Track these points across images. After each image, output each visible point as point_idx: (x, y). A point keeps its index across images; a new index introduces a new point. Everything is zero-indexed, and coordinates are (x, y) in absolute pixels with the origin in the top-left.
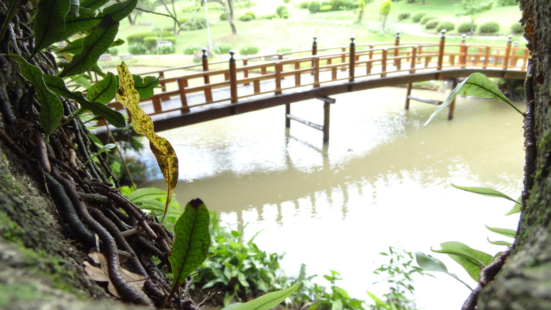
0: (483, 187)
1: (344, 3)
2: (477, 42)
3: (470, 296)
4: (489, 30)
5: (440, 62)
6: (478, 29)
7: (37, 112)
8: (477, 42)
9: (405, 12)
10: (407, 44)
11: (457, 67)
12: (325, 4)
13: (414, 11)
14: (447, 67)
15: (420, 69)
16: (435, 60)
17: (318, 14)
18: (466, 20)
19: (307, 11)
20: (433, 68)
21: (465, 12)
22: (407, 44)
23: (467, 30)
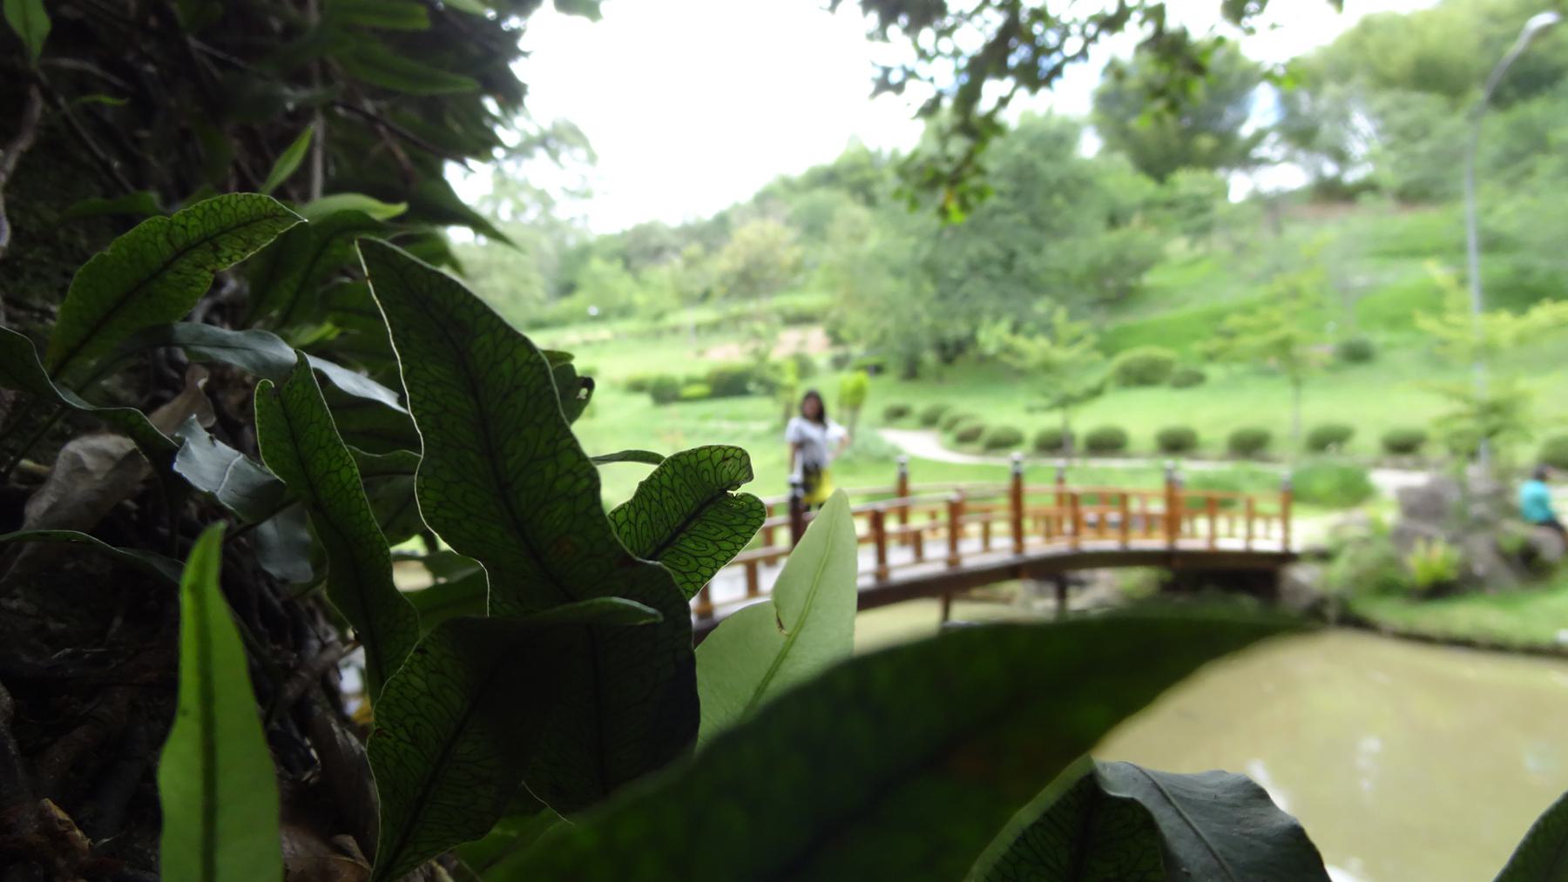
0: (1062, 774)
1: (1257, 66)
2: (1089, 474)
3: (624, 234)
4: (1107, 444)
5: (1018, 533)
6: (1080, 444)
7: (62, 626)
8: (1089, 474)
9: (897, 400)
10: (931, 491)
11: (1061, 546)
12: (691, 381)
13: (920, 401)
14: (1036, 546)
15: (973, 554)
16: (1001, 528)
17: (676, 409)
18: (1051, 421)
19: (643, 401)
20: (1002, 549)
21: (1043, 402)
22: (931, 491)
23: (1053, 445)
